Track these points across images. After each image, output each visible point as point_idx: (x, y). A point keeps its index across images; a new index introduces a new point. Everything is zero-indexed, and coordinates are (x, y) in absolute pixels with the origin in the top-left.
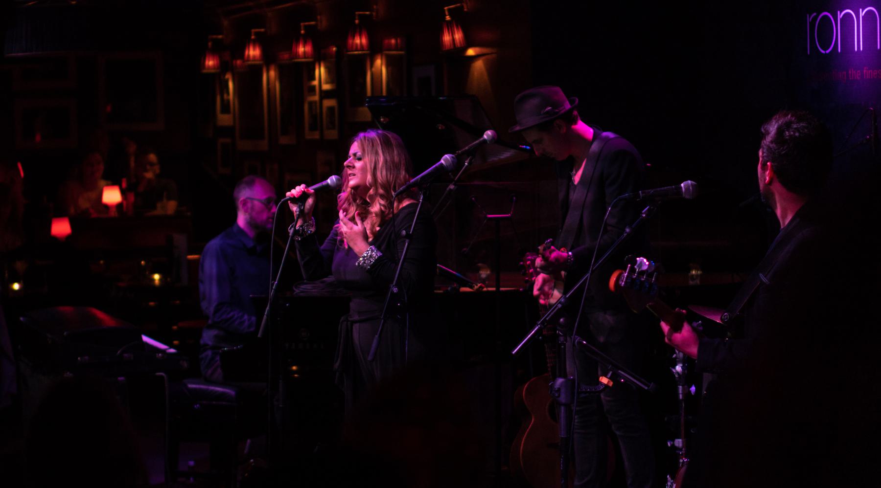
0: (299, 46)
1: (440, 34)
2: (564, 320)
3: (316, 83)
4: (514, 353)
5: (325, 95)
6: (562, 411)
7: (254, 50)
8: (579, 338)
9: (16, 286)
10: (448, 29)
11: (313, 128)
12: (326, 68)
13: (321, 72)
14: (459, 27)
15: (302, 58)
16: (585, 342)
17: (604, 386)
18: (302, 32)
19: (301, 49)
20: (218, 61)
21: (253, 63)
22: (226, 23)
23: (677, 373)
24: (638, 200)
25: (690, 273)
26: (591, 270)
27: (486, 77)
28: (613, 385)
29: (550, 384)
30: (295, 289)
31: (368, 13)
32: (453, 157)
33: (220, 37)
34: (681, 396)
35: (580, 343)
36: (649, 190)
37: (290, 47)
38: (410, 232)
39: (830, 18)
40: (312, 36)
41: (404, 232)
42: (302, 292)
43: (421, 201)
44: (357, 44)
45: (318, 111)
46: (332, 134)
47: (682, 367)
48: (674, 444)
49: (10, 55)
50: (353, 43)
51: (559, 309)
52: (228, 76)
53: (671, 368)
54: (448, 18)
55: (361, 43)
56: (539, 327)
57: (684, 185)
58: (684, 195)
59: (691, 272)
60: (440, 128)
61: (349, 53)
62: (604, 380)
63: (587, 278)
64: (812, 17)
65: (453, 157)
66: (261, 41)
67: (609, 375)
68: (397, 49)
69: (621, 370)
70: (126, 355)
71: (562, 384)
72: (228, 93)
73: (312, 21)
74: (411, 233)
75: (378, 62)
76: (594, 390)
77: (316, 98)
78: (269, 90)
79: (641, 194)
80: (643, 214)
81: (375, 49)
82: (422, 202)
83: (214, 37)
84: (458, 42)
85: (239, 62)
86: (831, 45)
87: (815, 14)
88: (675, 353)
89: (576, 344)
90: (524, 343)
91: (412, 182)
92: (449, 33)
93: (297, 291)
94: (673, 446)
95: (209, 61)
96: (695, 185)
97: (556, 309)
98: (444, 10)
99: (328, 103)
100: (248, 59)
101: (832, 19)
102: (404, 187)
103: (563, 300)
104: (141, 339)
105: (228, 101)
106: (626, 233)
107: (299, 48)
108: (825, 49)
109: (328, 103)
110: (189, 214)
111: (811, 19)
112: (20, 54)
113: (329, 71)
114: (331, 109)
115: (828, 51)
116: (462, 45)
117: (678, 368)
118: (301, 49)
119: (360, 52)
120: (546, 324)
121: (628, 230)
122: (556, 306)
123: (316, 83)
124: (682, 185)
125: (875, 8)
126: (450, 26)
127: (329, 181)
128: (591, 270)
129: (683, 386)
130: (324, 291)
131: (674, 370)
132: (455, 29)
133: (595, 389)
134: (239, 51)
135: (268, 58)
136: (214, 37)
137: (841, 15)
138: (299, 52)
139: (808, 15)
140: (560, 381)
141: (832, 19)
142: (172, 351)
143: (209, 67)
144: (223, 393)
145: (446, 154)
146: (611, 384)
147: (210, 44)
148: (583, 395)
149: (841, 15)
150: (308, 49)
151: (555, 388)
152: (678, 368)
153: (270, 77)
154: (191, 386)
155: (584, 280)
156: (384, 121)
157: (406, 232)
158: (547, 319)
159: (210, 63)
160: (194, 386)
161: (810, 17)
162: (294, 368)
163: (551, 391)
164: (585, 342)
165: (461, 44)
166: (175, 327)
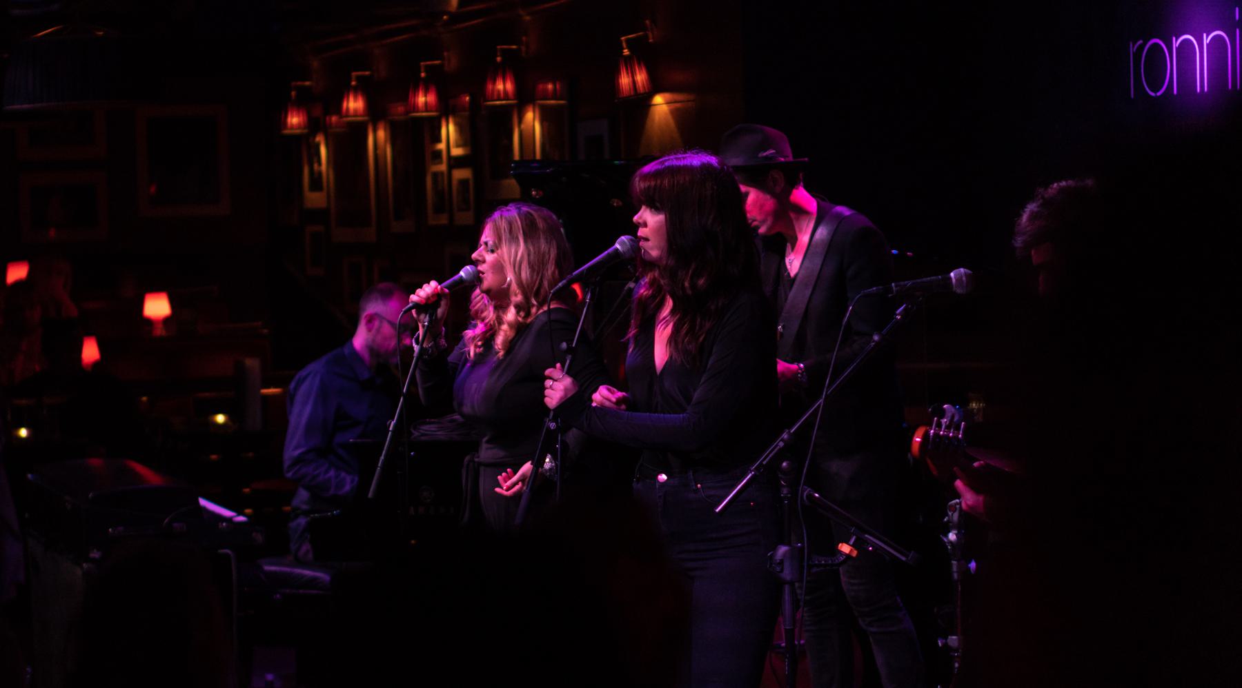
0: (418, 94)
1: (617, 74)
4: (717, 510)
5: (455, 162)
6: (787, 592)
7: (356, 100)
8: (808, 490)
9: (23, 433)
10: (627, 70)
12: (456, 124)
13: (449, 130)
15: (422, 112)
16: (817, 495)
17: (844, 557)
18: (423, 75)
22: (315, 64)
23: (951, 542)
26: (824, 393)
28: (857, 555)
29: (769, 554)
30: (413, 431)
31: (514, 47)
32: (631, 240)
33: (307, 83)
34: (956, 576)
35: (810, 497)
36: (906, 282)
38: (572, 344)
39: (1161, 47)
40: (437, 81)
41: (564, 345)
42: (423, 435)
44: (499, 91)
45: (446, 182)
46: (465, 218)
47: (956, 535)
48: (946, 643)
50: (493, 91)
51: (780, 449)
52: (320, 138)
53: (941, 536)
54: (626, 52)
56: (753, 475)
58: (954, 289)
59: (971, 404)
60: (615, 204)
62: (845, 548)
63: (819, 405)
64: (1136, 47)
65: (631, 240)
66: (365, 88)
67: (851, 542)
71: (784, 555)
72: (320, 163)
73: (437, 59)
75: (529, 116)
76: (830, 562)
77: (443, 167)
79: (894, 288)
81: (524, 97)
82: (589, 302)
84: (640, 85)
85: (334, 119)
86: (1163, 85)
87: (1141, 41)
88: (947, 515)
91: (576, 275)
92: (628, 73)
93: (416, 434)
94: (945, 645)
95: (292, 117)
97: (776, 450)
98: (621, 42)
99: (460, 174)
100: (347, 115)
104: (198, 502)
105: (320, 173)
106: (874, 341)
107: (418, 97)
108: (1155, 91)
109: (460, 174)
110: (266, 331)
112: (25, 106)
114: (464, 183)
115: (1158, 94)
116: (647, 91)
117: (952, 536)
118: (421, 99)
119: (504, 102)
121: (876, 338)
122: (777, 445)
123: (442, 146)
125: (1227, 35)
126: (629, 64)
127: (462, 273)
128: (824, 393)
129: (958, 561)
131: (946, 540)
133: (832, 561)
135: (375, 113)
136: (299, 83)
137: (1176, 43)
138: (418, 104)
139: (1131, 43)
140: (783, 550)
142: (242, 518)
143: (292, 127)
144: (315, 579)
145: (623, 235)
146: (855, 554)
147: (293, 93)
148: (815, 570)
149: (1176, 43)
150: (431, 98)
151: (776, 560)
152: (952, 536)
153: (378, 139)
154: (267, 568)
155: (815, 409)
156: (537, 195)
158: (764, 463)
159: (294, 120)
160: (273, 568)
161: (1133, 47)
163: (771, 564)
164: (817, 495)
166: (247, 490)
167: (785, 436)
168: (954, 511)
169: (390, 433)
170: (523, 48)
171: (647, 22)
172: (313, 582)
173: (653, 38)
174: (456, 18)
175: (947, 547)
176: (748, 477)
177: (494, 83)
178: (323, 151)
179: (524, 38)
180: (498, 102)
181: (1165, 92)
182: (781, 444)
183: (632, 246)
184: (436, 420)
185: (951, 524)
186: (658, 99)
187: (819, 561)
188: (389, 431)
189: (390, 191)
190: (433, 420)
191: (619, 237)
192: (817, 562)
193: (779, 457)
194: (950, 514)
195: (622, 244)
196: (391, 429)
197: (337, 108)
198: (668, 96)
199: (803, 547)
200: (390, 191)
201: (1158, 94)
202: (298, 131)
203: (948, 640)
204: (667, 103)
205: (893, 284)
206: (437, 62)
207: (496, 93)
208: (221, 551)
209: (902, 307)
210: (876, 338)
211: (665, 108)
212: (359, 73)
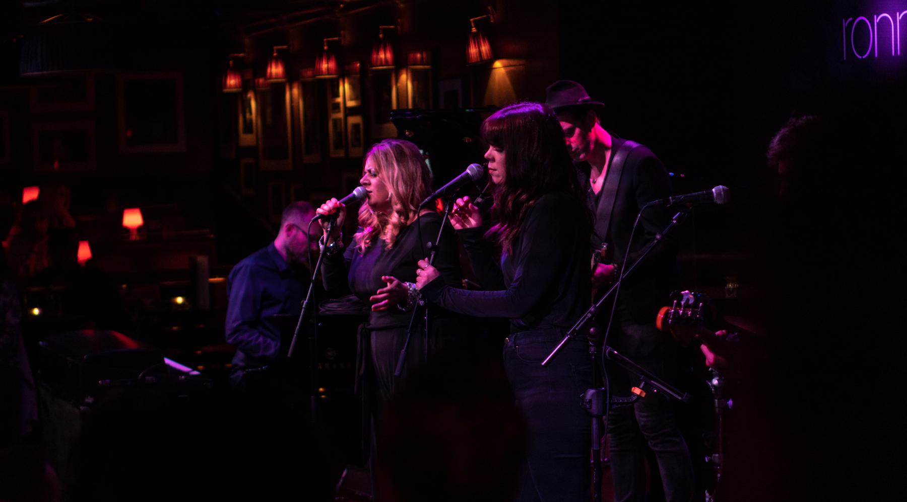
0: (322, 61)
1: (467, 47)
2: (594, 330)
3: (340, 100)
4: (543, 364)
5: (350, 112)
7: (276, 67)
10: (475, 43)
11: (338, 146)
12: (351, 84)
13: (345, 88)
14: (486, 39)
15: (325, 75)
16: (616, 352)
18: (326, 48)
19: (325, 66)
20: (240, 80)
21: (276, 80)
24: (668, 206)
25: (726, 286)
27: (507, 80)
28: (646, 396)
30: (321, 309)
33: (242, 55)
34: (717, 410)
35: (611, 353)
37: (313, 63)
40: (336, 52)
42: (327, 311)
43: (446, 211)
44: (381, 59)
47: (718, 380)
49: (25, 74)
50: (377, 58)
51: (589, 318)
52: (251, 95)
54: (474, 30)
55: (386, 58)
57: (716, 190)
58: (715, 200)
59: (728, 285)
60: (467, 141)
61: (374, 68)
62: (637, 391)
66: (283, 58)
67: (641, 386)
68: (422, 63)
69: (653, 380)
70: (147, 378)
71: (593, 395)
74: (437, 244)
75: (404, 77)
76: (626, 401)
77: (341, 115)
78: (292, 108)
80: (673, 220)
81: (400, 64)
83: (236, 55)
85: (261, 81)
87: (851, 19)
89: (607, 354)
90: (550, 354)
92: (475, 46)
93: (323, 310)
95: (231, 79)
96: (726, 190)
97: (585, 320)
98: (470, 22)
99: (353, 120)
100: (271, 77)
101: (869, 24)
102: (429, 197)
103: (593, 310)
104: (164, 362)
105: (251, 120)
108: (862, 55)
109: (353, 120)
111: (847, 24)
112: (36, 73)
113: (353, 87)
114: (356, 126)
118: (325, 66)
119: (385, 67)
120: (575, 334)
121: (658, 237)
122: (586, 316)
123: (340, 100)
124: (714, 190)
127: (355, 192)
129: (718, 399)
130: (350, 309)
131: (710, 384)
132: (482, 44)
134: (262, 71)
135: (291, 76)
136: (236, 55)
137: (877, 20)
140: (591, 392)
141: (869, 24)
142: (196, 373)
143: (231, 87)
145: (472, 163)
146: (644, 395)
147: (231, 62)
148: (615, 407)
149: (877, 20)
150: (332, 65)
153: (293, 95)
157: (432, 244)
158: (577, 329)
159: (232, 82)
161: (845, 22)
162: (321, 389)
164: (616, 352)
165: (487, 56)
166: (199, 352)
167: (592, 309)
169: (303, 310)
171: (490, 8)
177: (378, 53)
178: (253, 104)
182: (589, 315)
183: (478, 171)
186: (498, 64)
191: (469, 165)
196: (304, 306)
197: (263, 72)
198: (505, 61)
204: (504, 67)
206: (336, 38)
209: (677, 215)
211: (503, 70)
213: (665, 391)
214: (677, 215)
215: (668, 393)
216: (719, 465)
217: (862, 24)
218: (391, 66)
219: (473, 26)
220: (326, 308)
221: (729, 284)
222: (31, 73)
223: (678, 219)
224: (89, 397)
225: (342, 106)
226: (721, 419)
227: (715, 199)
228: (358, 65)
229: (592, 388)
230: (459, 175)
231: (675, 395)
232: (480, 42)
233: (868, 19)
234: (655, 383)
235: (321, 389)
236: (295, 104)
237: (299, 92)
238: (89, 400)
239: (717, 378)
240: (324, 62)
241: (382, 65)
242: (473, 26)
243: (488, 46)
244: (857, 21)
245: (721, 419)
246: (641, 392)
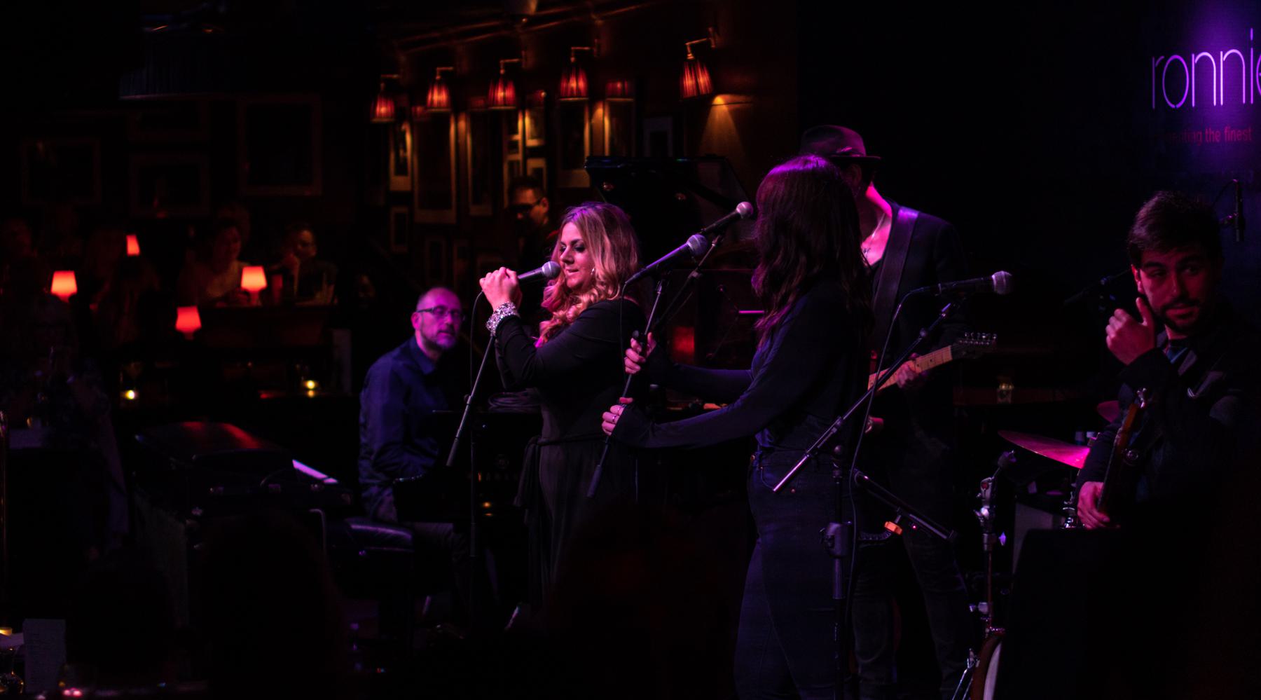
0: (498, 90)
1: (681, 77)
3: (518, 137)
4: (775, 490)
5: (530, 153)
7: (440, 93)
8: (858, 472)
9: (131, 395)
12: (533, 118)
13: (525, 123)
14: (705, 68)
15: (501, 106)
16: (866, 477)
18: (502, 72)
19: (500, 94)
21: (437, 110)
23: (983, 516)
30: (491, 403)
31: (586, 48)
32: (702, 239)
33: (395, 76)
35: (860, 479)
37: (485, 89)
40: (515, 77)
42: (499, 407)
44: (572, 89)
45: (521, 169)
47: (989, 510)
48: (977, 609)
50: (567, 88)
54: (690, 56)
55: (578, 88)
57: (996, 277)
58: (995, 290)
60: (679, 198)
61: (563, 100)
62: (891, 526)
65: (702, 239)
66: (449, 83)
67: (897, 521)
69: (912, 514)
70: (271, 485)
71: (835, 531)
72: (405, 149)
77: (519, 157)
78: (457, 144)
81: (595, 95)
83: (388, 76)
84: (703, 86)
85: (419, 109)
87: (1163, 57)
88: (980, 491)
92: (691, 76)
94: (976, 611)
95: (380, 107)
97: (829, 435)
98: (686, 46)
99: (534, 163)
103: (838, 423)
105: (405, 159)
107: (497, 92)
109: (534, 163)
112: (138, 97)
115: (1178, 106)
117: (985, 511)
118: (500, 94)
119: (576, 99)
122: (830, 431)
123: (518, 137)
124: (993, 277)
125: (1242, 53)
126: (693, 67)
131: (978, 514)
132: (701, 75)
134: (420, 95)
135: (457, 106)
136: (388, 76)
137: (1195, 59)
138: (497, 97)
140: (834, 527)
145: (694, 234)
146: (900, 531)
147: (382, 85)
149: (1195, 59)
150: (509, 93)
152: (985, 511)
153: (459, 128)
154: (354, 527)
158: (818, 447)
159: (382, 110)
160: (359, 527)
161: (1155, 61)
162: (487, 505)
164: (866, 477)
167: (838, 422)
168: (987, 488)
169: (467, 407)
170: (595, 50)
171: (710, 29)
172: (394, 540)
173: (715, 44)
174: (534, 20)
175: (979, 520)
176: (803, 460)
177: (568, 81)
178: (408, 138)
179: (596, 40)
180: (571, 99)
181: (1184, 103)
182: (835, 430)
183: (701, 244)
184: (511, 393)
185: (983, 500)
186: (719, 100)
187: (866, 537)
188: (466, 404)
189: (470, 177)
190: (508, 393)
191: (691, 235)
192: (871, 539)
193: (834, 440)
194: (983, 490)
195: (693, 242)
196: (468, 403)
197: (422, 98)
198: (728, 97)
199: (852, 525)
200: (470, 177)
201: (1178, 106)
202: (385, 120)
203: (979, 607)
204: (727, 104)
205: (939, 285)
206: (516, 60)
207: (569, 92)
208: (313, 510)
209: (947, 307)
210: (923, 334)
211: (725, 108)
212: (443, 68)
213: (927, 528)
214: (947, 307)
215: (930, 530)
216: (986, 616)
217: (1176, 65)
218: (583, 97)
219: (689, 51)
220: (498, 404)
221: (1002, 385)
222: (133, 97)
223: (949, 312)
224: (197, 508)
225: (520, 144)
226: (990, 558)
227: (995, 287)
228: (543, 94)
229: (836, 522)
230: (677, 248)
231: (938, 533)
232: (698, 71)
233: (1185, 60)
234: (915, 517)
235: (487, 505)
236: (461, 140)
237: (466, 125)
238: (198, 512)
239: (988, 507)
240: (500, 90)
241: (572, 96)
242: (689, 51)
243: (708, 77)
244: (1171, 59)
245: (990, 558)
246: (897, 528)
